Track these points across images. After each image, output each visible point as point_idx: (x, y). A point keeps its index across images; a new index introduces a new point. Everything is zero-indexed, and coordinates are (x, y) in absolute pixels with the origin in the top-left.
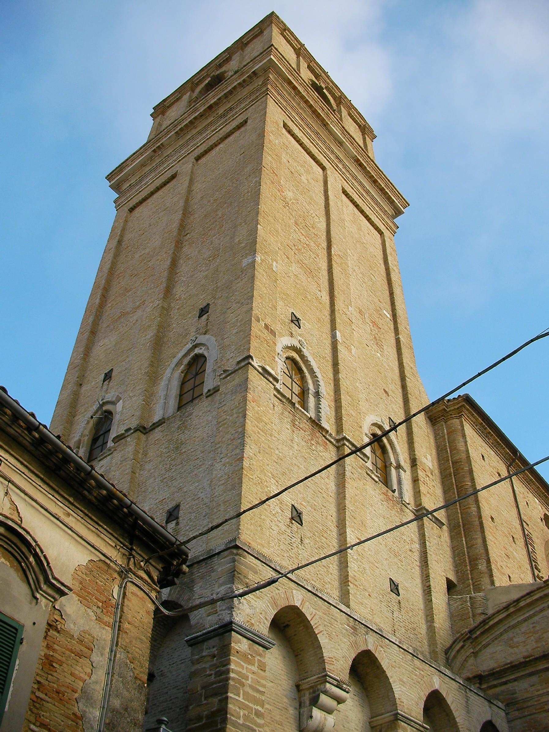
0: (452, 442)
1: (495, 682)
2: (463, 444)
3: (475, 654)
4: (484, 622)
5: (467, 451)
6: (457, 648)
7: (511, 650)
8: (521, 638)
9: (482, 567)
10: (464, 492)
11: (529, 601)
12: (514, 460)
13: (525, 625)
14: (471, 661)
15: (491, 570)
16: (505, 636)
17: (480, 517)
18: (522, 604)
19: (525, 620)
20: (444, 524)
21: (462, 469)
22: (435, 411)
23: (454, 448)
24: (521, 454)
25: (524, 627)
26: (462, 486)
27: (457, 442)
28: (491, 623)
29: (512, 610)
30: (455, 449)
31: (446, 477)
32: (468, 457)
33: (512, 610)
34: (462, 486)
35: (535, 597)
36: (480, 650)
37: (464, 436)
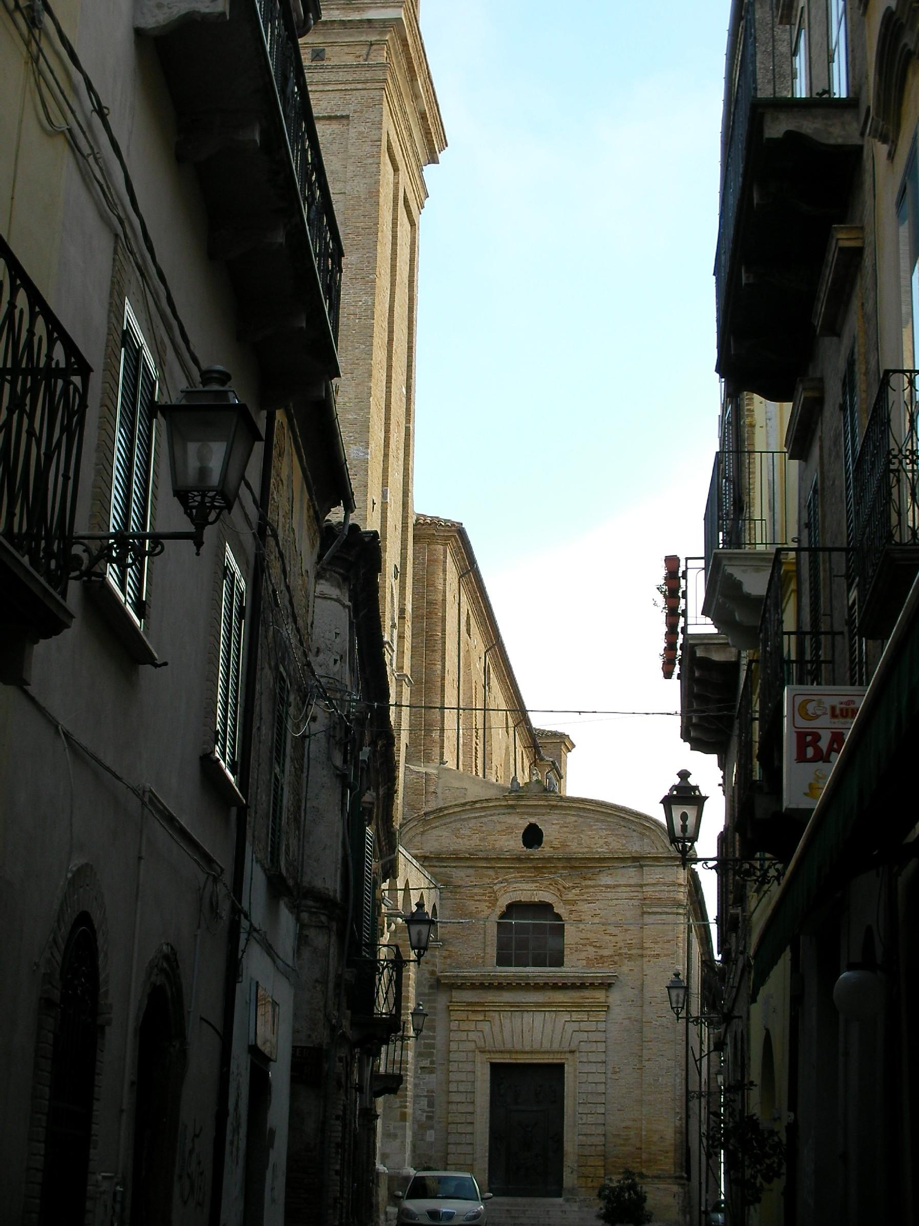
0: (431, 574)
1: (437, 864)
2: (442, 581)
3: (423, 833)
4: (441, 810)
5: (445, 592)
6: (411, 825)
7: (455, 839)
8: (468, 832)
9: (436, 735)
10: (432, 642)
11: (484, 805)
12: (468, 572)
13: (473, 821)
14: (418, 838)
15: (443, 741)
16: (453, 825)
17: (443, 678)
18: (478, 805)
19: (475, 818)
20: (260, 439)
21: (436, 614)
22: (423, 532)
23: (431, 585)
24: (477, 568)
25: (472, 823)
26: (432, 636)
27: (436, 576)
28: (446, 812)
29: (468, 807)
30: (433, 585)
31: (417, 617)
32: (444, 600)
33: (468, 807)
34: (432, 636)
35: (491, 804)
36: (428, 830)
37: (444, 571)
